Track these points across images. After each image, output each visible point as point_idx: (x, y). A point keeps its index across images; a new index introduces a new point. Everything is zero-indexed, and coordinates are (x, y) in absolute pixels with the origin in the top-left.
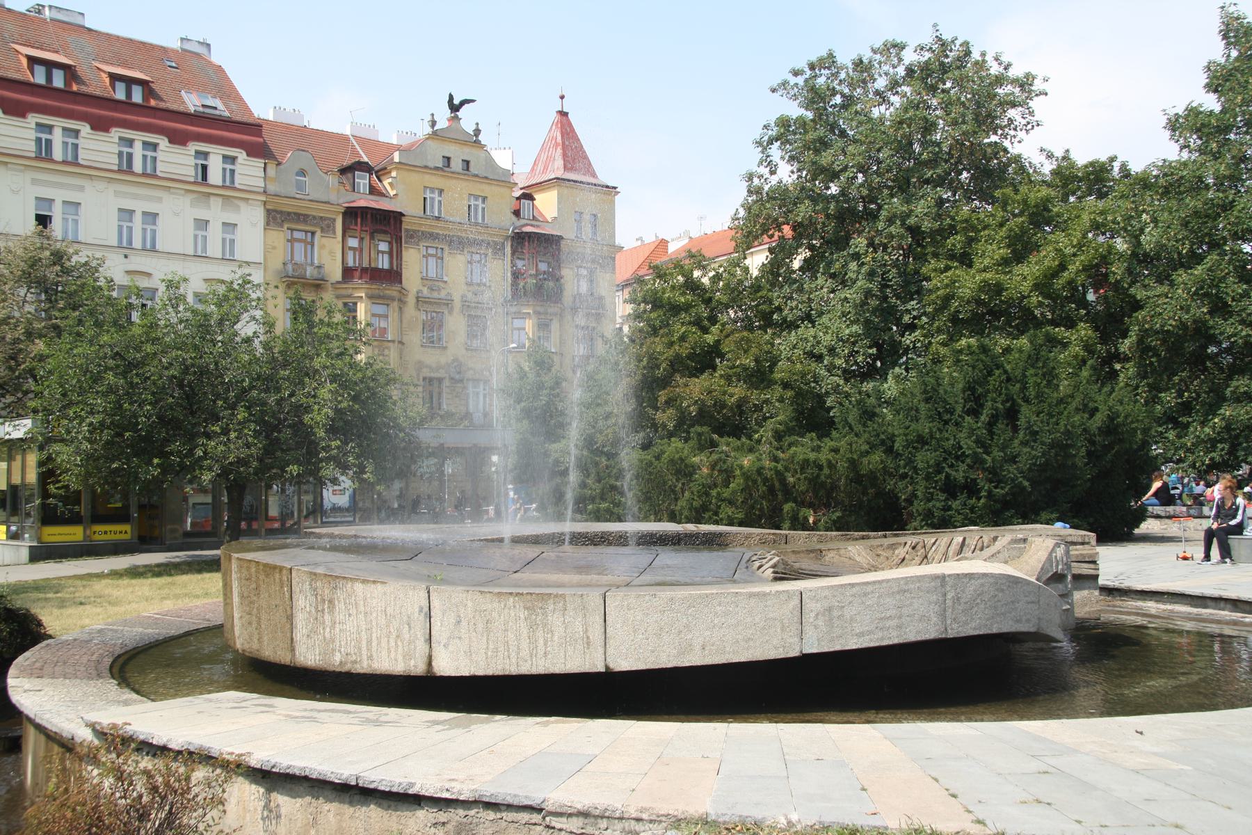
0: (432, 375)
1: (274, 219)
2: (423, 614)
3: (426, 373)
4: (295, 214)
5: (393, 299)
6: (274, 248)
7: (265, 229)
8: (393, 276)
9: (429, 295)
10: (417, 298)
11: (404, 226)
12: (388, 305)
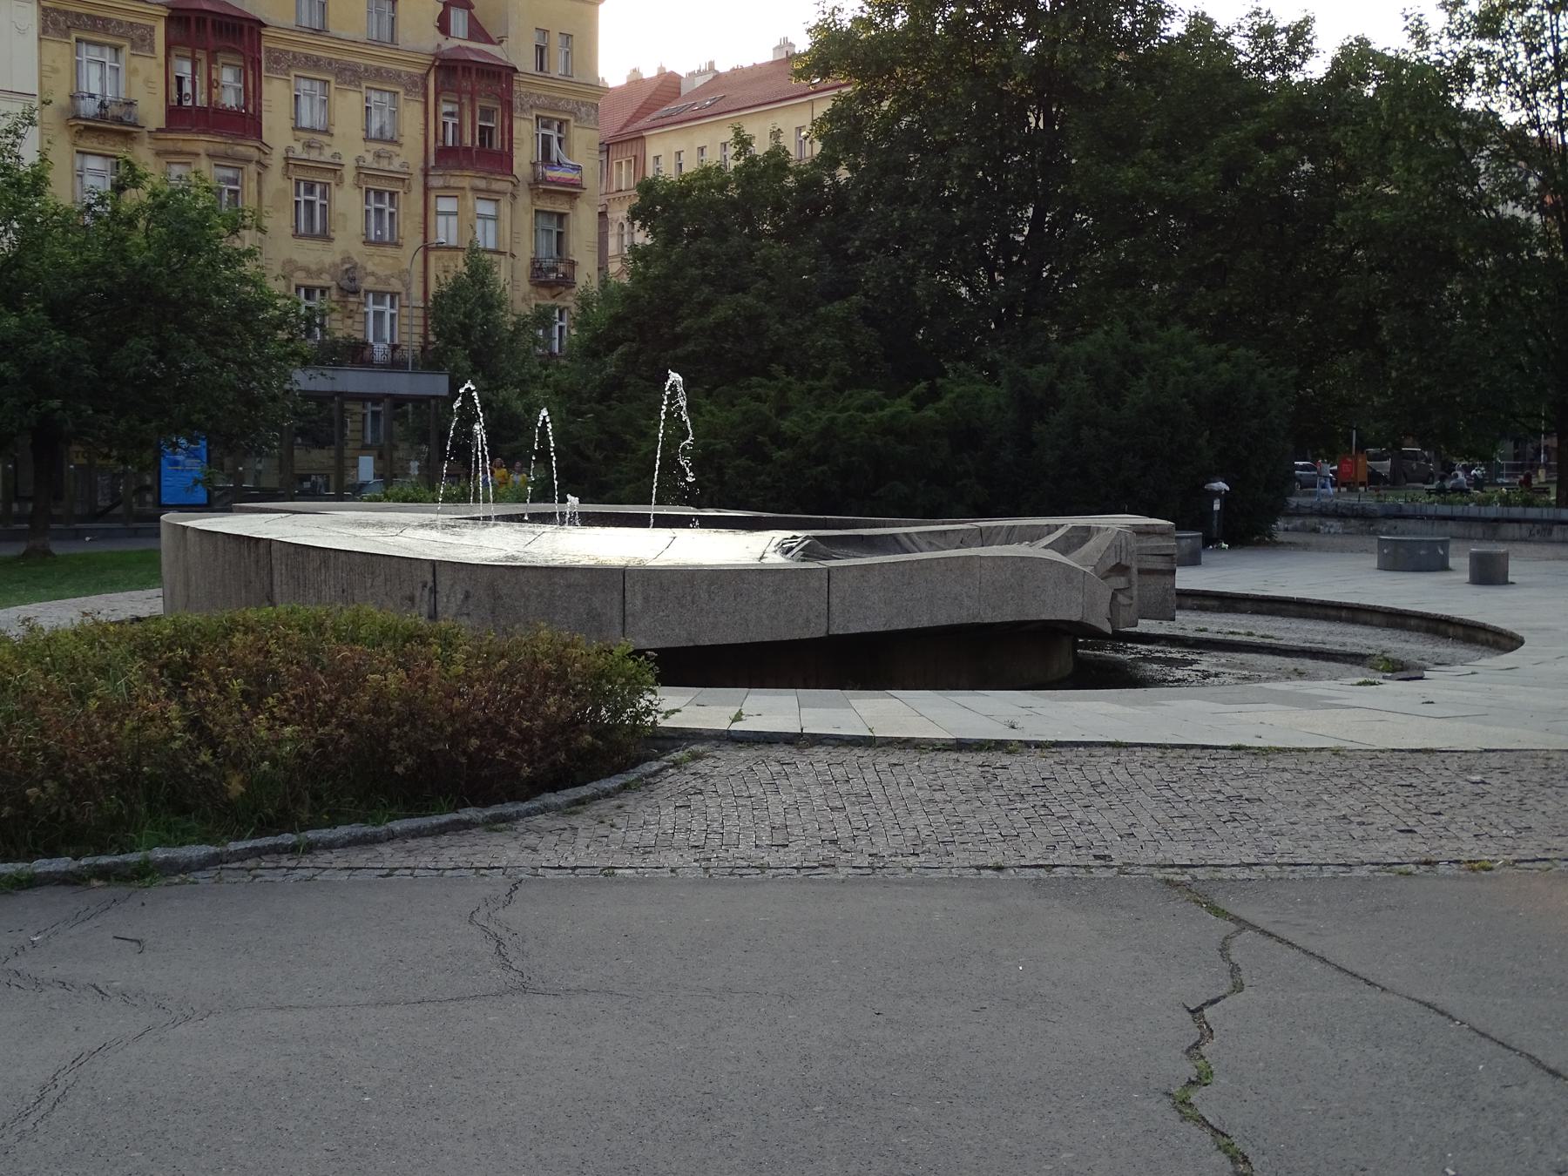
0: (309, 282)
1: (55, 23)
2: (427, 590)
3: (300, 278)
4: (88, 16)
5: (504, 193)
6: (55, 70)
7: (40, 39)
8: (246, 123)
9: (305, 156)
10: (287, 159)
11: (265, 44)
12: (497, 201)
